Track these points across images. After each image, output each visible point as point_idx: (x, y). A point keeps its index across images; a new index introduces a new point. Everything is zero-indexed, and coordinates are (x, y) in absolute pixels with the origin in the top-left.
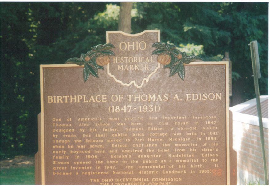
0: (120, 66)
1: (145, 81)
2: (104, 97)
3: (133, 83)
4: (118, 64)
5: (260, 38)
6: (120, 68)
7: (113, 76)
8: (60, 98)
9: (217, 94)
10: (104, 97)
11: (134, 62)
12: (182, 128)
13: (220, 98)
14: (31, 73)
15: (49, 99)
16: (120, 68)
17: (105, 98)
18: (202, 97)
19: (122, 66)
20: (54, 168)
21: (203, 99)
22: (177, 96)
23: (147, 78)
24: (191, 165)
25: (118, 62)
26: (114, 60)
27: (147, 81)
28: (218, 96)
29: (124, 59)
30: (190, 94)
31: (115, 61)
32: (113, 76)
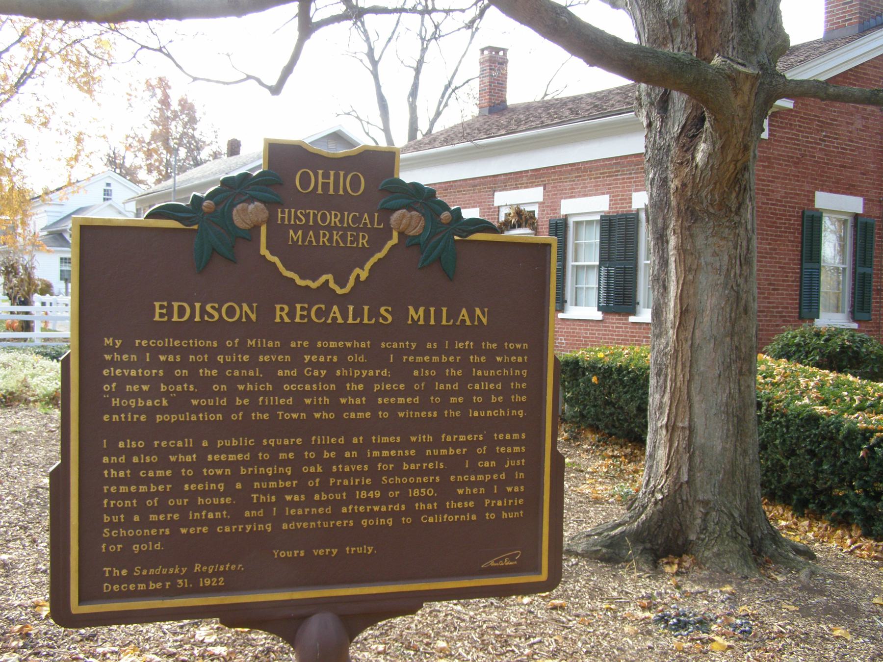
0: (296, 234)
1: (358, 275)
2: (161, 307)
3: (327, 281)
4: (290, 226)
5: (860, 210)
6: (295, 239)
7: (275, 259)
8: (282, 309)
9: (245, 307)
10: (161, 307)
11: (333, 224)
12: (250, 387)
13: (253, 317)
14: (456, 238)
15: (278, 313)
16: (295, 239)
17: (164, 311)
18: (203, 311)
19: (300, 232)
20: (106, 518)
21: (206, 318)
22: (466, 315)
23: (363, 270)
24: (242, 469)
25: (289, 220)
26: (280, 215)
27: (364, 275)
28: (249, 312)
29: (307, 216)
30: (165, 304)
31: (283, 219)
32: (275, 259)
